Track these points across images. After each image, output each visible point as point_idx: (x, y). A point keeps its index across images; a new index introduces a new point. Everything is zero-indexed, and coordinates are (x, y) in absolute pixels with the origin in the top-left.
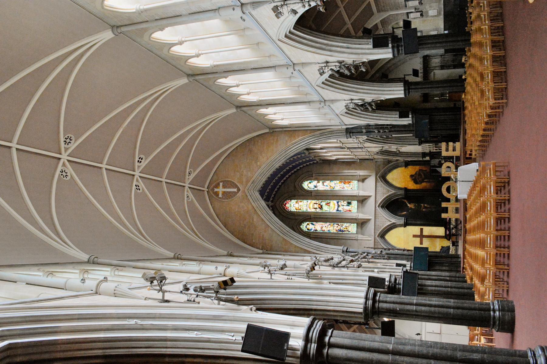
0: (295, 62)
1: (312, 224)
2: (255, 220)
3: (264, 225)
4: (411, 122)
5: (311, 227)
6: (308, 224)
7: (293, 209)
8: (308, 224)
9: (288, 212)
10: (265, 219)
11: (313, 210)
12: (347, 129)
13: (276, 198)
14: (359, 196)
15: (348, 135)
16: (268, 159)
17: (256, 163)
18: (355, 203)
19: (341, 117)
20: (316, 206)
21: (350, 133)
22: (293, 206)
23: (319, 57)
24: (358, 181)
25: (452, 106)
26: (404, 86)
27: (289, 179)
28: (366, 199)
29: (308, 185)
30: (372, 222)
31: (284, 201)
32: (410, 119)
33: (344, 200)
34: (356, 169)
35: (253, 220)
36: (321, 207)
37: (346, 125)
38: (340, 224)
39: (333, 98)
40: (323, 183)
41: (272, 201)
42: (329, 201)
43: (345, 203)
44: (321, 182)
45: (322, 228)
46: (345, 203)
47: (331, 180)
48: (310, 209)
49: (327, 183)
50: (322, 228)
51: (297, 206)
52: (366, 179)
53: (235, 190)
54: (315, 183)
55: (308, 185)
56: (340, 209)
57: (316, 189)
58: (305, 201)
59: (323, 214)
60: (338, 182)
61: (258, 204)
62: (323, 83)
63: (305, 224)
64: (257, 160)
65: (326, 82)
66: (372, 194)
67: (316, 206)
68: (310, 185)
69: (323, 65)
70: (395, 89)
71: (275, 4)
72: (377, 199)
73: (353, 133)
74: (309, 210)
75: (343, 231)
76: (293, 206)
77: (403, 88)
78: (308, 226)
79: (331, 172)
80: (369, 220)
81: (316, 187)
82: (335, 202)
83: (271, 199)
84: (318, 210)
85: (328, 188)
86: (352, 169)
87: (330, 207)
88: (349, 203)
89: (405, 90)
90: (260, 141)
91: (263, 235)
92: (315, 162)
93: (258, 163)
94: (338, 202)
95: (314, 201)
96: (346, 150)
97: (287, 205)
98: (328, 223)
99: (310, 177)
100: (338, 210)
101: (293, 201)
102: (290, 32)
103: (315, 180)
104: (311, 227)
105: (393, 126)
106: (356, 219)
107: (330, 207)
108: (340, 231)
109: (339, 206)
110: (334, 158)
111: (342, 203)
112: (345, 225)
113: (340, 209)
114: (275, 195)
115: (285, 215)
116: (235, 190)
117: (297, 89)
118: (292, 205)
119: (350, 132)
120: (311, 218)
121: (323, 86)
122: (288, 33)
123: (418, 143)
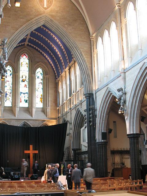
0: (126, 73)
1: (11, 74)
2: (21, 20)
3: (17, 26)
4: (97, 141)
5: (9, 73)
6: (11, 71)
8: (11, 71)
9: (20, 57)
10: (22, 28)
11: (21, 76)
12: (93, 94)
13: (31, 48)
14: (32, 108)
15: (87, 95)
16: (70, 33)
17: (67, 24)
18: (26, 105)
19: (105, 88)
21: (89, 97)
22: (24, 61)
23: (129, 88)
24: (43, 108)
25: (108, 171)
26: (137, 134)
27: (44, 58)
28: (30, 113)
29: (39, 71)
30: (13, 117)
31: (27, 53)
32: (100, 141)
33: (28, 97)
34: (51, 106)
35: (21, 18)
36: (23, 81)
37: (96, 93)
38: (11, 94)
39: (127, 79)
40: (41, 83)
41: (28, 45)
42: (28, 87)
43: (27, 99)
44: (42, 81)
46: (27, 99)
47: (43, 89)
49: (41, 86)
51: (24, 63)
52: (45, 113)
53: (45, 6)
54: (41, 77)
55: (39, 71)
57: (37, 78)
58: (28, 69)
59: (18, 82)
60: (42, 94)
61: (34, 23)
62: (109, 91)
63: (11, 69)
64: (69, 25)
65: (80, 113)
66: (34, 117)
69: (124, 91)
70: (135, 127)
71: (124, 90)
72: (30, 121)
73: (89, 99)
74: (21, 72)
75: (6, 96)
76: (24, 61)
77: (135, 133)
79: (50, 89)
80: (15, 116)
81: (38, 77)
82: (27, 91)
83: (30, 44)
84: (21, 79)
85: (37, 86)
86: (51, 103)
87: (23, 88)
88: (26, 101)
89: (133, 134)
90: (83, 28)
91: (9, 26)
92: (57, 77)
93: (66, 26)
94: (27, 93)
95: (27, 77)
96: (69, 98)
97: (25, 57)
98: (11, 86)
99: (45, 73)
100: (21, 93)
101: (27, 61)
102: (111, 94)
103: (44, 77)
104: (9, 73)
105: (95, 129)
106: (15, 105)
107: (23, 88)
108: (6, 95)
109: (24, 94)
110: (60, 91)
111: (27, 96)
112: (11, 98)
114: (33, 47)
115: (18, 54)
116: (45, 6)
117: (140, 48)
118: (24, 60)
119: (90, 97)
120: (15, 73)
121: (107, 92)
122: (111, 92)
123: (74, 148)
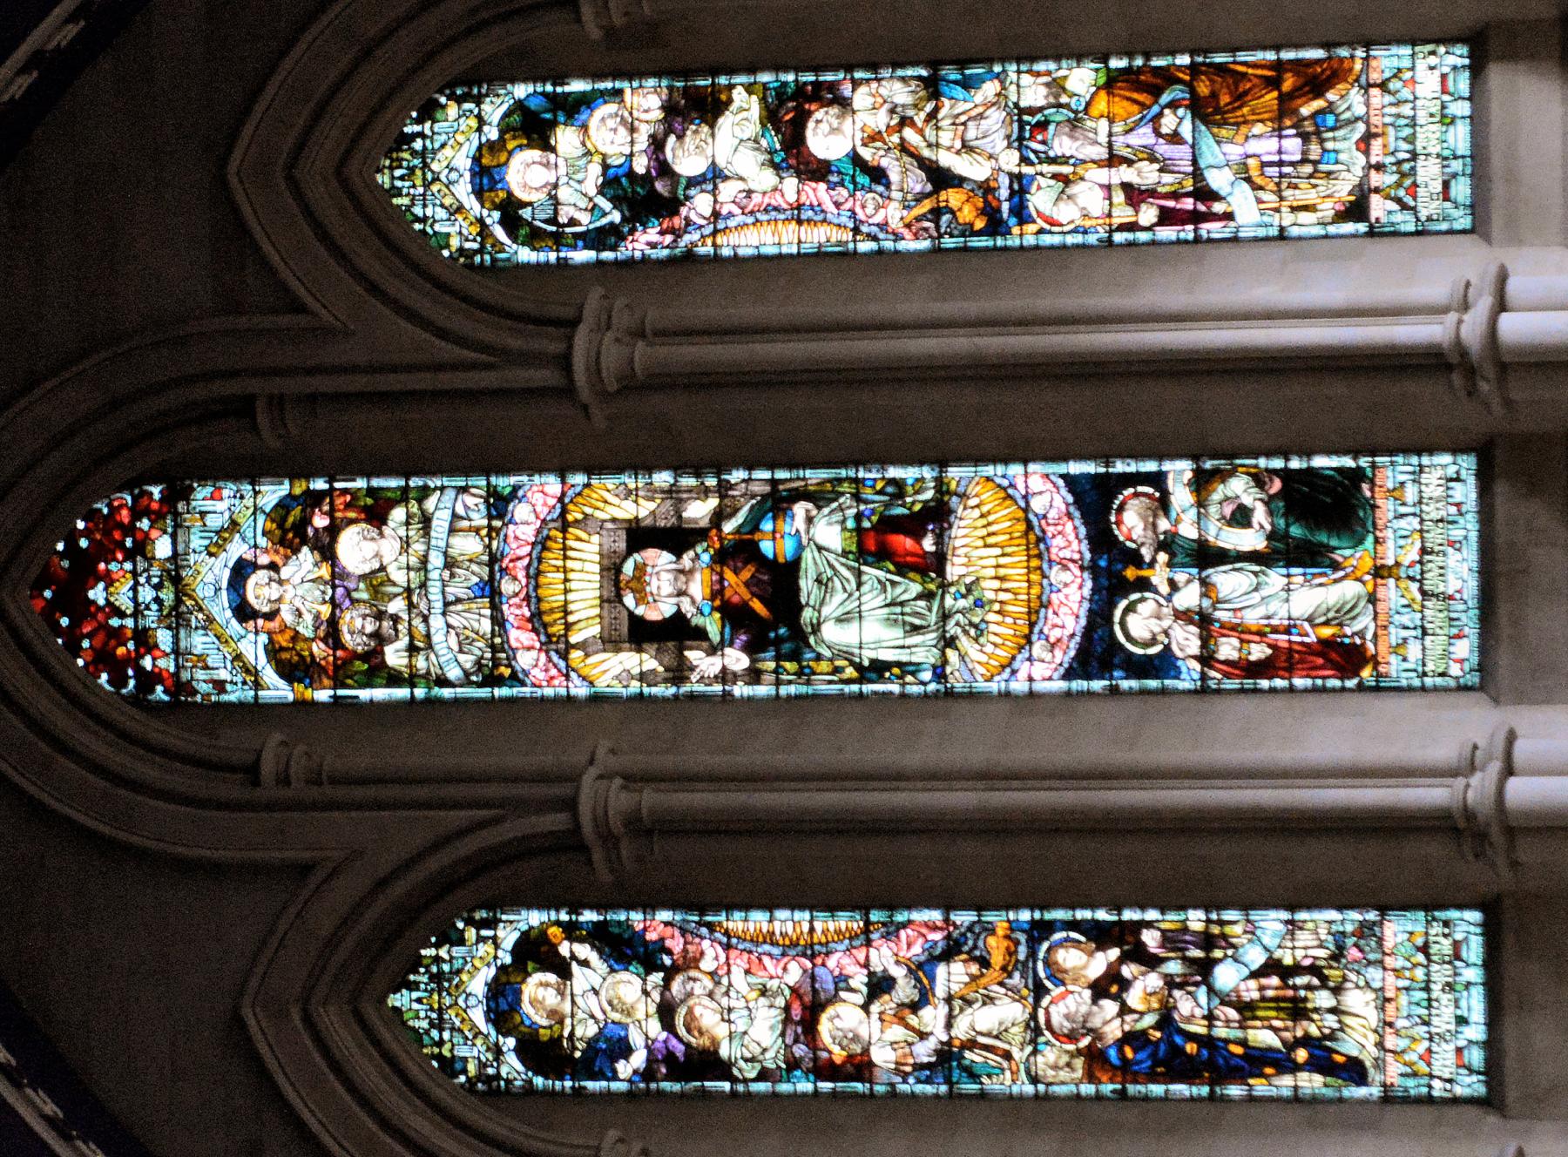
1: (623, 949)
7: (226, 659)
8: (535, 952)
20: (672, 586)
36: (770, 610)
40: (786, 123)
45: (806, 1011)
48: (557, 645)
50: (806, 1011)
56: (1141, 623)
67: (672, 586)
68: (525, 174)
78: (538, 991)
94: (1094, 500)
100: (1098, 651)
109: (1115, 573)
113: (1141, 623)
